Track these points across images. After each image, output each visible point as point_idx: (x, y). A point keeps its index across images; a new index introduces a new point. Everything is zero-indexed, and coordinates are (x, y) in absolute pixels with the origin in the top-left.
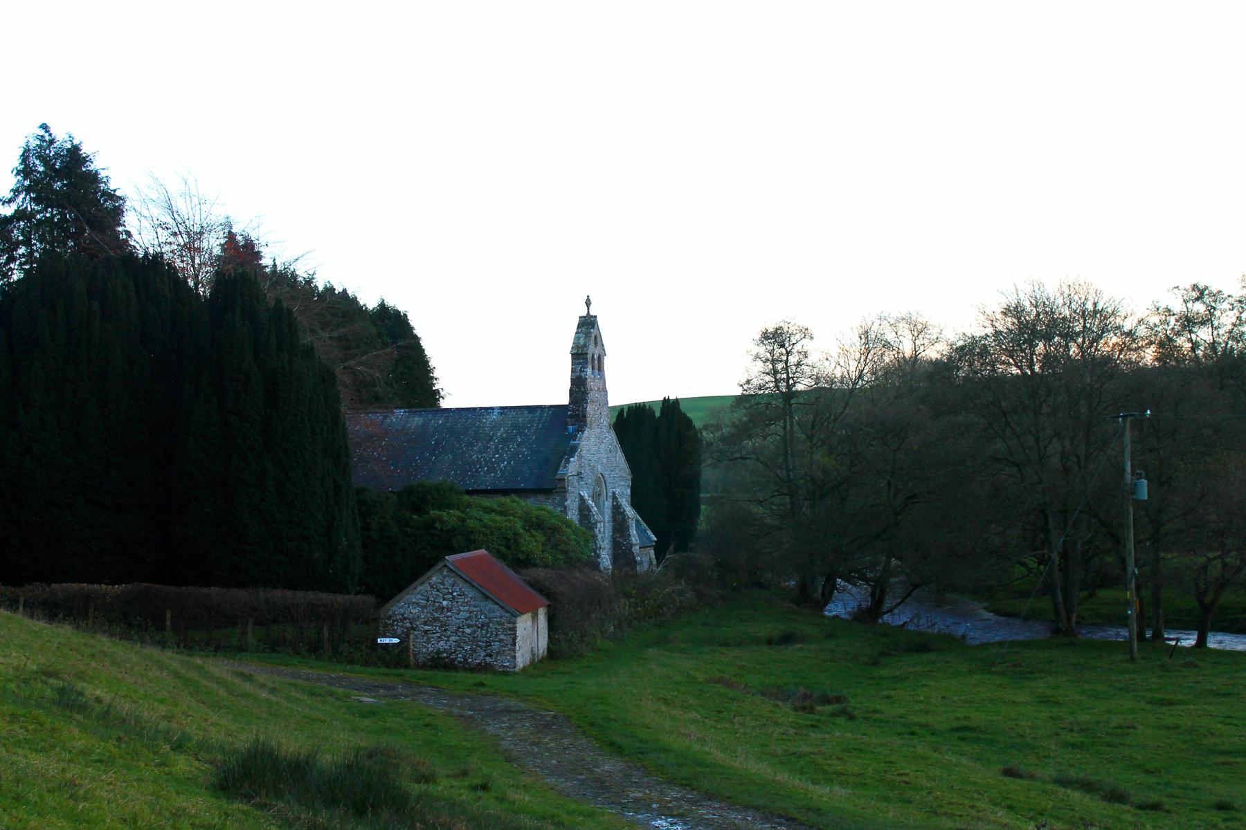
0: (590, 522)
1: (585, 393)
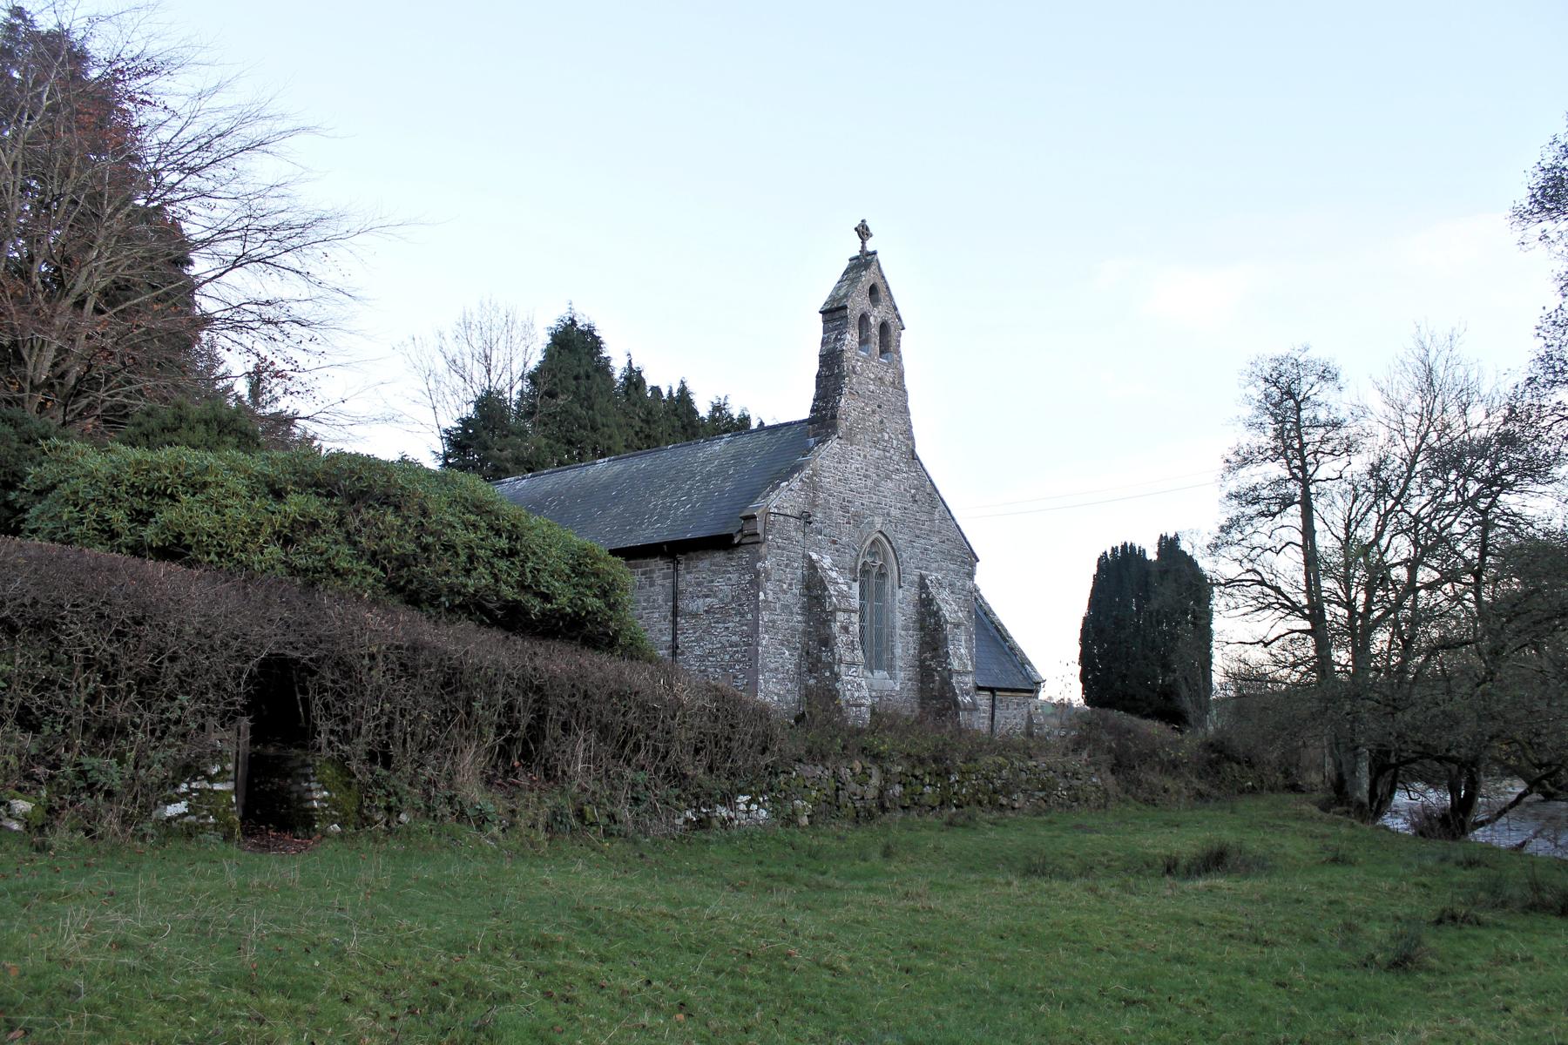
0: (824, 611)
1: (840, 377)
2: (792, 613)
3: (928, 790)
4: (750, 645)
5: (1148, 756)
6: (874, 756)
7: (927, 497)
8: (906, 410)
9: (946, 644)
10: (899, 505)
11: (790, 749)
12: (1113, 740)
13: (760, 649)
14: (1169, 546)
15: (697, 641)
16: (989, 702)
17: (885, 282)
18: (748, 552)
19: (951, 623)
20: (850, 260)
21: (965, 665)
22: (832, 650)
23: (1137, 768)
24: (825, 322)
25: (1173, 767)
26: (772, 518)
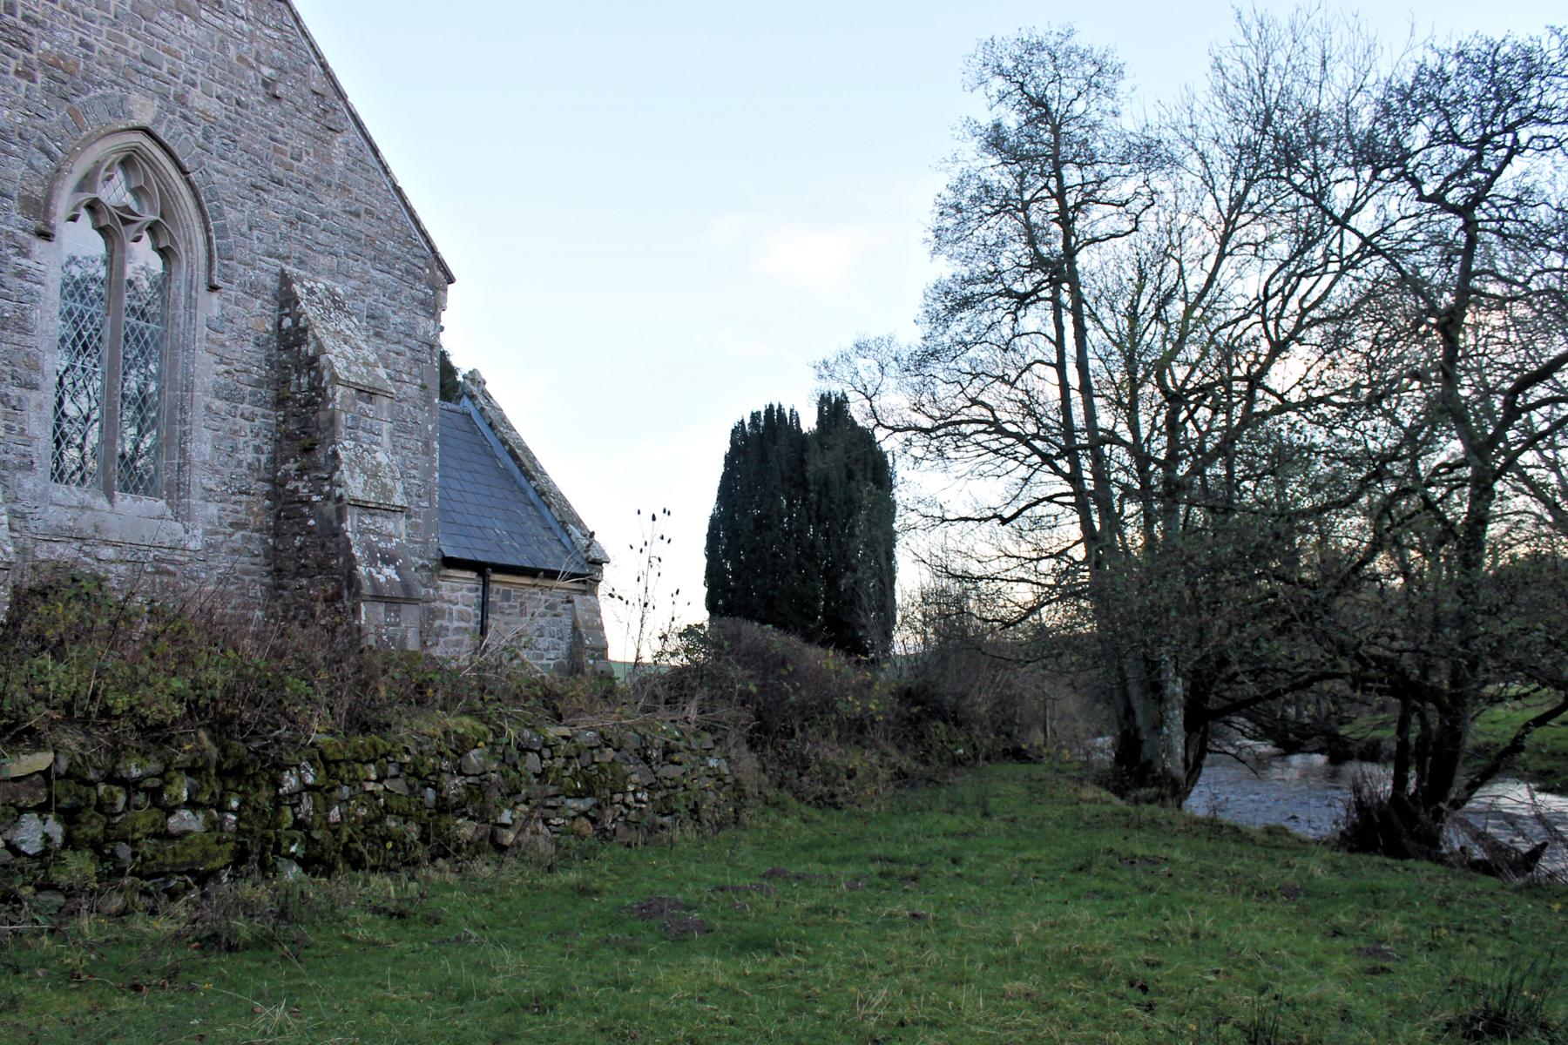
3: (184, 820)
5: (819, 710)
10: (218, 89)
12: (751, 677)
14: (833, 411)
16: (475, 597)
19: (348, 384)
23: (798, 734)
25: (856, 731)
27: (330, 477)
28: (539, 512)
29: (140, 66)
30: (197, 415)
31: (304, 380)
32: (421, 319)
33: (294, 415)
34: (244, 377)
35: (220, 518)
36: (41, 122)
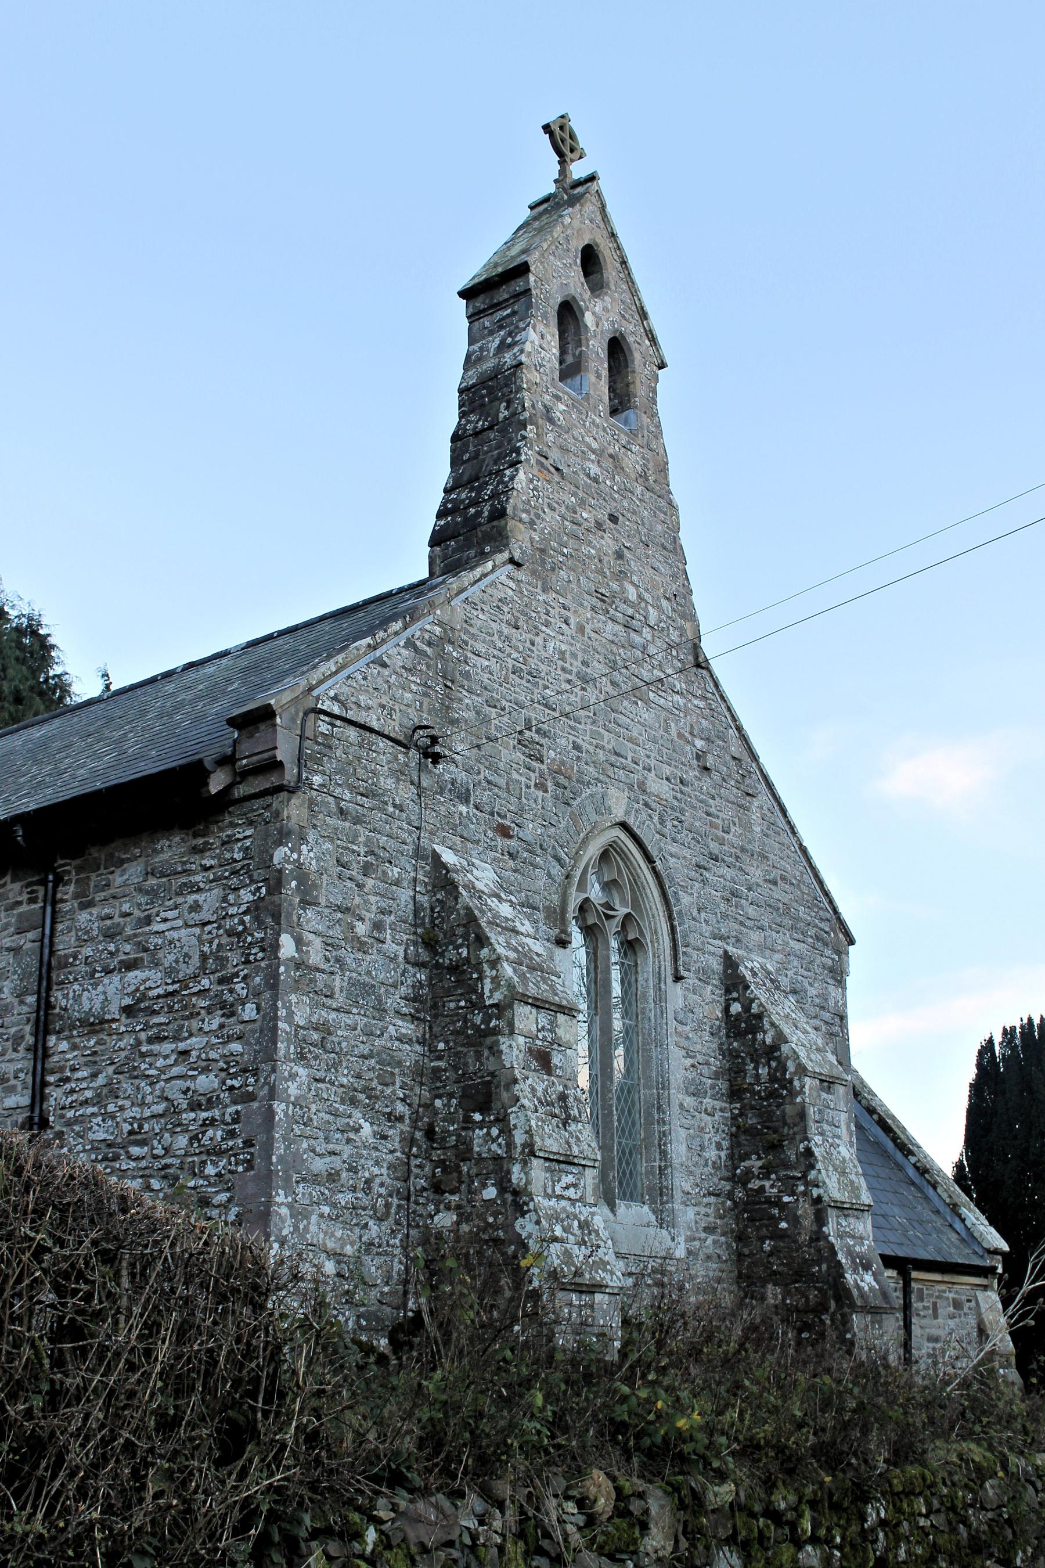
2: (381, 1010)
4: (251, 1097)
6: (650, 1454)
7: (732, 763)
8: (674, 549)
9: (805, 1130)
10: (667, 770)
11: (360, 1437)
13: (279, 1108)
15: (98, 1100)
17: (619, 248)
18: (251, 823)
19: (814, 1076)
20: (532, 208)
21: (855, 1190)
22: (502, 1120)
24: (473, 317)
26: (324, 728)
27: (805, 1176)
28: (921, 1191)
29: (613, 758)
30: (674, 1114)
31: (763, 1071)
32: (831, 988)
33: (753, 1108)
34: (705, 1070)
35: (696, 1222)
36: (553, 830)
